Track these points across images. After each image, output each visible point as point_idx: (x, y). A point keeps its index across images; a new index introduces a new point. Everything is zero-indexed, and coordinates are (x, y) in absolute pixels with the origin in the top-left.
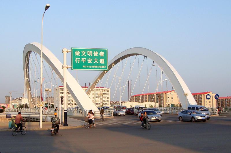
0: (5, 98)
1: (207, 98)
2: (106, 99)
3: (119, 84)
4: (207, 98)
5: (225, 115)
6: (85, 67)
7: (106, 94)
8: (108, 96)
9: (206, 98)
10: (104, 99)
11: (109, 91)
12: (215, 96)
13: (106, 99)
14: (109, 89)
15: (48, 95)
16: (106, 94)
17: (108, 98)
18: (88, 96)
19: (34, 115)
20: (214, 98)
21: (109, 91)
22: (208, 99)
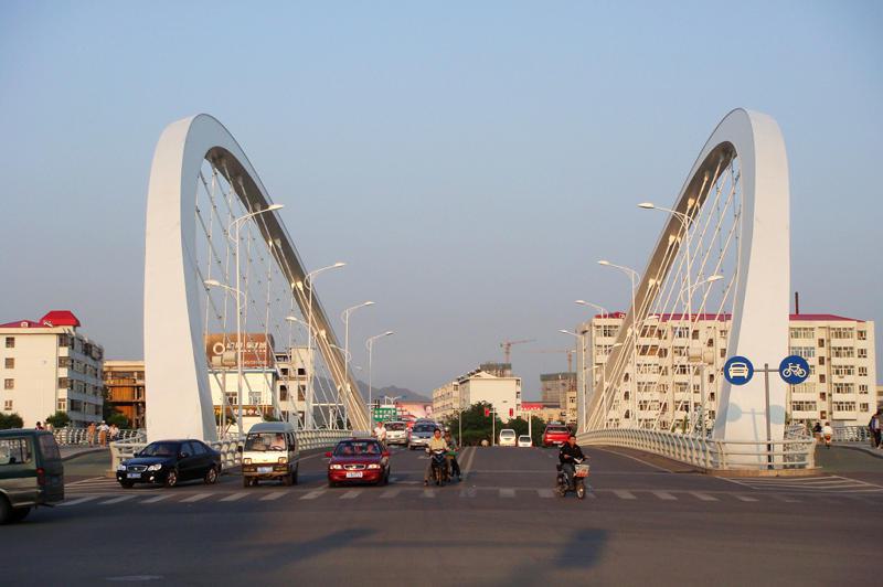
0: (541, 384)
1: (732, 375)
2: (848, 379)
3: (732, 292)
4: (732, 375)
5: (153, 464)
6: (241, 183)
7: (849, 351)
8: (862, 363)
9: (727, 376)
10: (836, 379)
11: (870, 335)
12: (784, 365)
13: (848, 379)
14: (869, 327)
15: (507, 353)
16: (849, 351)
17: (863, 372)
18: (146, 370)
19: (867, 484)
20: (775, 378)
21: (870, 335)
22: (740, 381)
